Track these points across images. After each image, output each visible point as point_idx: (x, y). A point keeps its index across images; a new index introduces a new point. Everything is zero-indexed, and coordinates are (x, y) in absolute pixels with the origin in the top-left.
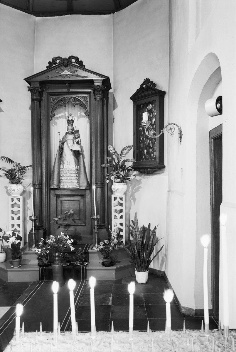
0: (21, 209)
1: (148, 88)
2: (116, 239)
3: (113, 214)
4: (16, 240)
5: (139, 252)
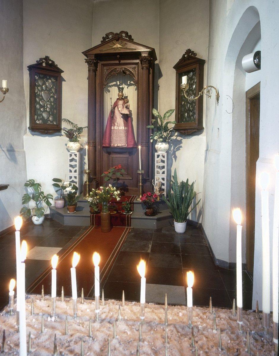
0: (77, 163)
1: (189, 58)
2: (158, 192)
3: (156, 169)
4: (71, 189)
5: (178, 205)
